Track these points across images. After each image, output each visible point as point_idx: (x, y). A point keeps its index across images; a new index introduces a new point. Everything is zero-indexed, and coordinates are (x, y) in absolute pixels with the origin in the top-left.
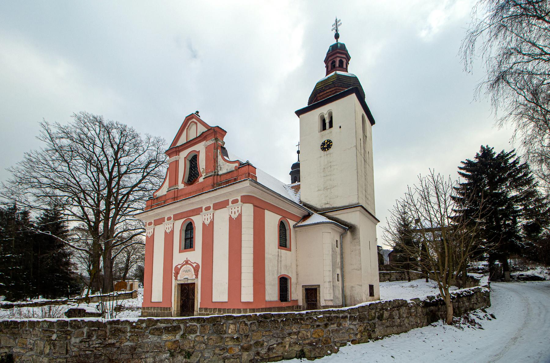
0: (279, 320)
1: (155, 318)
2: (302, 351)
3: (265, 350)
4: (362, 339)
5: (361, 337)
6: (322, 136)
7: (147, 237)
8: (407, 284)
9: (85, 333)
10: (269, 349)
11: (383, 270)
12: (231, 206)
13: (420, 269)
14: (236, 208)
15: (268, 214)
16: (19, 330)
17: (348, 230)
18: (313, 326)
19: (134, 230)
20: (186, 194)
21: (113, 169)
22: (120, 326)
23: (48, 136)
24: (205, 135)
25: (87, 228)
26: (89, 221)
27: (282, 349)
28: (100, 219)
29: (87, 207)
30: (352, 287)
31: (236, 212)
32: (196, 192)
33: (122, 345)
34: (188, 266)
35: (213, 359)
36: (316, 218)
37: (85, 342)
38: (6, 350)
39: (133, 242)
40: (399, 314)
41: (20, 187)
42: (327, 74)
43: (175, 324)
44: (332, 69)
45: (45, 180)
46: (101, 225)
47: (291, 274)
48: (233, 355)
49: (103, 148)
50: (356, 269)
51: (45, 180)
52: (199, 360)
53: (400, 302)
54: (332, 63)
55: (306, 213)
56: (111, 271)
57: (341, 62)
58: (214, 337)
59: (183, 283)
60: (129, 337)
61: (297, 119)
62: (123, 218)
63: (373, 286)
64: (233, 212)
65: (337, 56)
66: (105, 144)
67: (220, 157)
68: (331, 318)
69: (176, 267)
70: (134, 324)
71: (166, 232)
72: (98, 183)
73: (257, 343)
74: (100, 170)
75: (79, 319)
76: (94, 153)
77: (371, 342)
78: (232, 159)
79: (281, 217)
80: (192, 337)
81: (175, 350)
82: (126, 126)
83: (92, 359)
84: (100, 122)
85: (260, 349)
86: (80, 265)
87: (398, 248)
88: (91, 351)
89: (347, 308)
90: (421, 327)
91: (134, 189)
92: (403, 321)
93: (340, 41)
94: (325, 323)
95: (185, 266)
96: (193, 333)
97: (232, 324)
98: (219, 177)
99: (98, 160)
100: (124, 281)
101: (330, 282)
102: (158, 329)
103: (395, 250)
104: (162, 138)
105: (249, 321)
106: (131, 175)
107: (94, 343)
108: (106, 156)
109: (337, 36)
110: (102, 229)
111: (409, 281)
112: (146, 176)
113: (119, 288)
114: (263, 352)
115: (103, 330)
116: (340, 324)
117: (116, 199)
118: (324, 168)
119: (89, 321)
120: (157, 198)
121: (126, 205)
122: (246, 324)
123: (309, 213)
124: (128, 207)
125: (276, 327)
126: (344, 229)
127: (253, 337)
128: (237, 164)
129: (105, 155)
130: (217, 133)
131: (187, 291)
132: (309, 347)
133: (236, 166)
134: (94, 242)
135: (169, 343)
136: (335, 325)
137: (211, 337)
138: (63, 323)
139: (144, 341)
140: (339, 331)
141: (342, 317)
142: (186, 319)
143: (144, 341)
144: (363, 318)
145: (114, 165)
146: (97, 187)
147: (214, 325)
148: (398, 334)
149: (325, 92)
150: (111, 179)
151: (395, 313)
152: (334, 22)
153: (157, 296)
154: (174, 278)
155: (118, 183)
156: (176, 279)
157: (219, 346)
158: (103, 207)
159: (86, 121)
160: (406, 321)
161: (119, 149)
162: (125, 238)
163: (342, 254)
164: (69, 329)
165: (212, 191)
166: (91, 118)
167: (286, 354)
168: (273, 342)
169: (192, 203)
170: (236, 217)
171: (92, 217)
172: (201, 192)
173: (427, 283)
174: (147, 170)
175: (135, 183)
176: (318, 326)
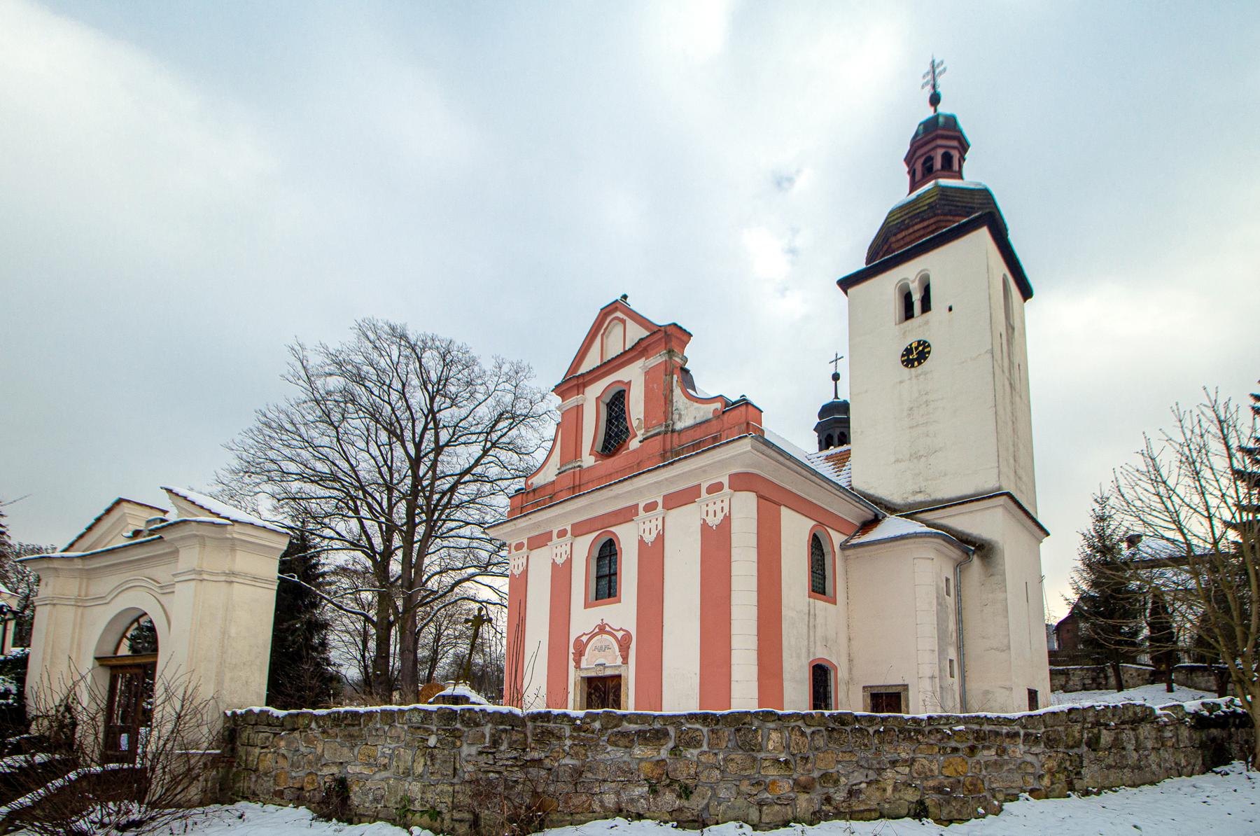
0: (871, 731)
2: (921, 803)
4: (1054, 790)
5: (1053, 783)
13: (1146, 658)
16: (361, 730)
17: (974, 552)
18: (944, 748)
20: (600, 479)
21: (422, 436)
22: (551, 725)
23: (302, 373)
24: (644, 344)
27: (878, 794)
30: (986, 693)
31: (719, 511)
32: (623, 471)
34: (605, 636)
36: (893, 526)
37: (488, 753)
38: (335, 770)
40: (1137, 739)
41: (247, 479)
43: (657, 726)
44: (924, 176)
45: (293, 467)
47: (837, 659)
50: (997, 649)
51: (293, 467)
52: (708, 805)
53: (1138, 710)
55: (870, 516)
57: (947, 159)
58: (738, 756)
59: (593, 674)
60: (570, 747)
63: (1036, 692)
67: (677, 392)
69: (578, 639)
70: (578, 722)
71: (554, 564)
72: (390, 469)
73: (825, 776)
77: (1074, 797)
80: (692, 753)
84: (403, 337)
85: (832, 790)
92: (1146, 756)
93: (943, 108)
94: (970, 744)
96: (695, 747)
98: (676, 435)
102: (625, 734)
108: (409, 407)
109: (935, 100)
112: (489, 450)
114: (839, 797)
116: (1004, 751)
117: (428, 499)
118: (911, 409)
119: (495, 712)
120: (534, 490)
122: (803, 734)
123: (876, 516)
124: (448, 519)
125: (866, 745)
126: (966, 552)
128: (718, 405)
130: (671, 338)
132: (936, 797)
136: (993, 752)
139: (598, 758)
140: (1001, 766)
141: (1008, 735)
143: (598, 758)
144: (1055, 740)
145: (425, 429)
147: (738, 730)
148: (1134, 785)
152: (928, 68)
154: (572, 664)
155: (433, 466)
156: (578, 666)
157: (748, 777)
160: (1153, 757)
163: (959, 612)
164: (458, 726)
167: (887, 806)
168: (858, 777)
169: (616, 497)
170: (717, 522)
172: (636, 471)
175: (467, 466)
176: (955, 750)
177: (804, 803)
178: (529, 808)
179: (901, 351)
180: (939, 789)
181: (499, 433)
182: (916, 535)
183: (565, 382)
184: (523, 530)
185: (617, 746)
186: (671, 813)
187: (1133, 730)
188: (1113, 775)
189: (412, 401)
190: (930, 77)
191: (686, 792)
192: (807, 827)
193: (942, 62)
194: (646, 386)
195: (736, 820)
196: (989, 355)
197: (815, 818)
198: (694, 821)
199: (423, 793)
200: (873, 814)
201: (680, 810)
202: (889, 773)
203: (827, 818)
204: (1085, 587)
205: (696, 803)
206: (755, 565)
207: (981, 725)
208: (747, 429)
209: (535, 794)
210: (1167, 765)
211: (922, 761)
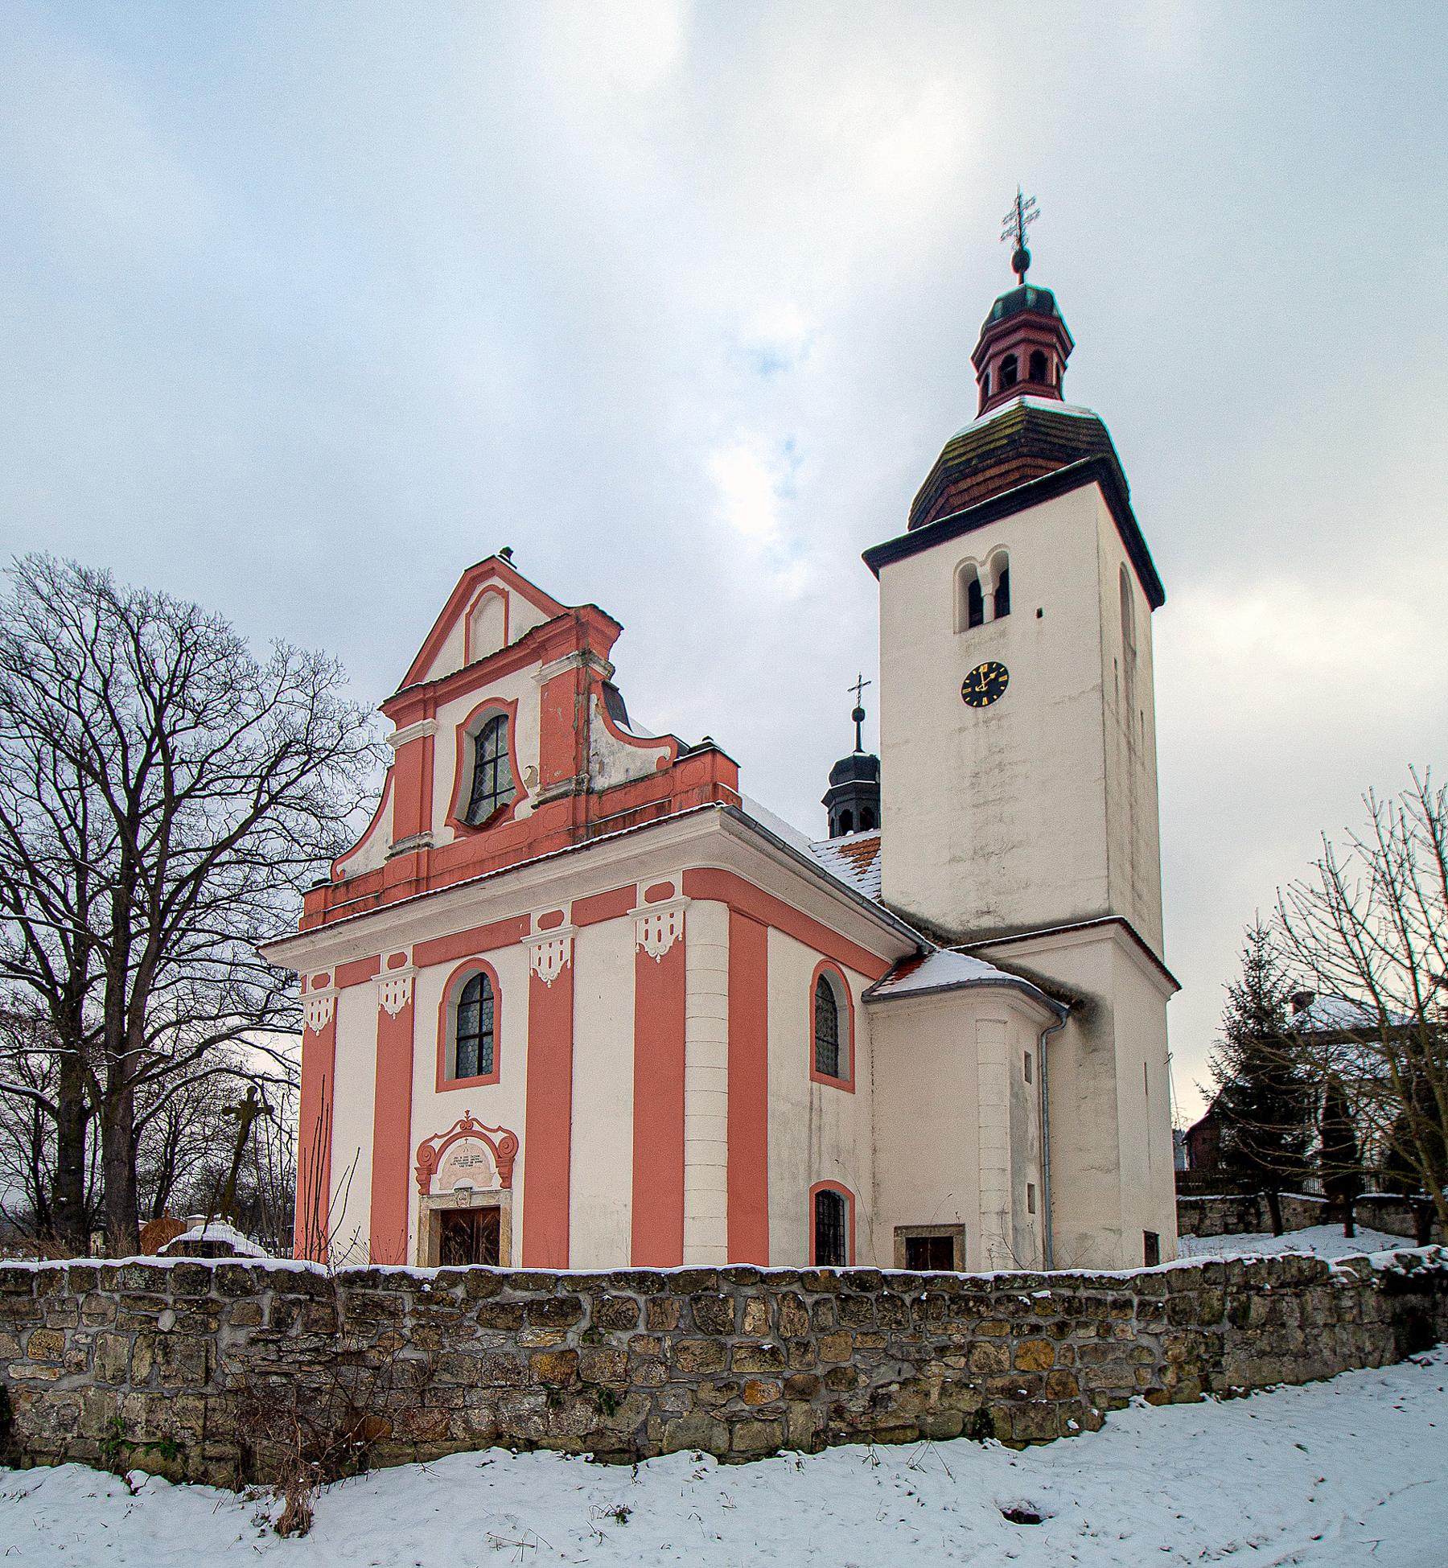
0: (908, 1300)
2: (982, 1413)
3: (862, 1402)
5: (1179, 1380)
6: (968, 650)
9: (267, 1312)
13: (1316, 1185)
14: (666, 918)
15: (776, 941)
16: (34, 1301)
18: (1019, 1326)
20: (464, 868)
22: (380, 1292)
24: (540, 637)
27: (917, 1401)
30: (1084, 1237)
31: (666, 932)
32: (504, 856)
36: (946, 967)
40: (1303, 1311)
43: (562, 1293)
52: (645, 1424)
53: (1305, 1265)
54: (1002, 368)
55: (910, 950)
57: (1039, 365)
58: (696, 1342)
59: (452, 1205)
64: (653, 935)
65: (1024, 338)
67: (598, 724)
69: (425, 1145)
71: (382, 1011)
72: (82, 833)
80: (619, 1339)
81: (564, 1385)
85: (846, 1396)
88: (286, 1375)
92: (1316, 1337)
95: (461, 1141)
96: (625, 1329)
98: (594, 798)
102: (505, 1308)
109: (1021, 262)
114: (856, 1406)
116: (1109, 1329)
117: (154, 891)
118: (976, 775)
120: (347, 884)
122: (800, 1305)
123: (919, 948)
125: (899, 1323)
126: (1057, 1013)
127: (824, 1350)
128: (666, 751)
130: (585, 631)
132: (1006, 1404)
135: (545, 1359)
137: (686, 1343)
138: (196, 1273)
139: (461, 1347)
140: (1104, 1353)
143: (461, 1347)
144: (1183, 1311)
145: (147, 763)
148: (1298, 1382)
152: (1011, 207)
154: (415, 1187)
155: (163, 832)
156: (425, 1191)
157: (711, 1377)
160: (1325, 1338)
163: (1044, 1108)
164: (214, 1294)
167: (930, 1420)
168: (885, 1373)
169: (492, 901)
170: (664, 951)
171: (59, 964)
173: (1350, 1241)
176: (1035, 1329)
180: (1010, 1392)
181: (284, 779)
183: (402, 693)
184: (328, 952)
185: (493, 1327)
187: (1297, 1295)
188: (1268, 1367)
190: (1013, 223)
191: (609, 1403)
194: (544, 711)
196: (1098, 694)
197: (818, 1442)
198: (622, 1451)
199: (150, 1411)
201: (600, 1432)
202: (934, 1368)
203: (837, 1441)
204: (1230, 1073)
205: (626, 1421)
206: (724, 1026)
207: (1075, 1289)
209: (352, 1411)
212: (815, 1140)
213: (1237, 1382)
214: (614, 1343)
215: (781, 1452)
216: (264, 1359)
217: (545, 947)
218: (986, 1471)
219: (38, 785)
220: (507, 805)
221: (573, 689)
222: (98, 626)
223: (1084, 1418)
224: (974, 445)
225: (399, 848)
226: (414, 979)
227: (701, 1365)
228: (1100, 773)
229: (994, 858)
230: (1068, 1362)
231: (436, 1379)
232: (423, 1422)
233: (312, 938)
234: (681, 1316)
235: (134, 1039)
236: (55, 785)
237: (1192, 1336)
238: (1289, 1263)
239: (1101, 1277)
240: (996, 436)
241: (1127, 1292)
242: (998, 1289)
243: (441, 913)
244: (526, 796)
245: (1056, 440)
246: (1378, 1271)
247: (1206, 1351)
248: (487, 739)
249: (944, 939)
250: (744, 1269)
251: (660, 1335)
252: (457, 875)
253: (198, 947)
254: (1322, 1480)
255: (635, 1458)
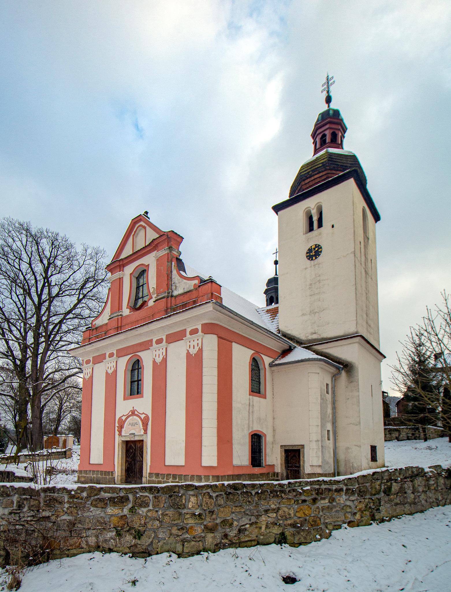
0: (253, 492)
1: (98, 486)
2: (283, 534)
5: (362, 517)
6: (308, 240)
7: (84, 379)
8: (422, 444)
10: (240, 531)
11: (389, 425)
12: (189, 338)
13: (440, 424)
15: (236, 348)
17: (342, 369)
18: (298, 501)
19: (68, 369)
20: (132, 323)
22: (56, 495)
25: (12, 367)
26: (14, 359)
27: (256, 530)
28: (28, 356)
29: (13, 340)
30: (347, 448)
32: (145, 319)
33: (59, 519)
34: (135, 417)
35: (170, 541)
36: (300, 353)
37: (15, 513)
39: (66, 385)
40: (413, 486)
42: (316, 151)
43: (122, 494)
46: (29, 363)
48: (194, 537)
49: (30, 264)
50: (353, 424)
52: (152, 542)
53: (414, 470)
54: (321, 138)
55: (286, 347)
56: (41, 424)
57: (334, 136)
58: (170, 512)
59: (128, 439)
61: (274, 217)
62: (54, 355)
64: (192, 347)
65: (330, 128)
66: (32, 259)
67: (174, 272)
68: (321, 491)
69: (120, 419)
70: (73, 493)
71: (107, 373)
72: (25, 309)
74: (27, 293)
75: (8, 484)
76: (20, 270)
77: (374, 524)
78: (190, 274)
79: (253, 352)
80: (143, 511)
82: (57, 234)
83: (23, 535)
84: (27, 230)
85: (228, 530)
86: (4, 415)
87: (410, 394)
88: (23, 525)
89: (341, 478)
90: (443, 506)
91: (68, 317)
92: (419, 496)
94: (313, 497)
95: (131, 417)
96: (145, 507)
97: (193, 495)
98: (173, 299)
99: (25, 279)
100: (56, 435)
101: (318, 441)
102: (102, 500)
103: (407, 397)
104: (101, 248)
105: (214, 492)
106: (64, 299)
107: (26, 515)
108: (34, 274)
109: (328, 100)
110: (30, 367)
111: (426, 440)
112: (81, 300)
113: (51, 444)
114: (232, 533)
115: (37, 500)
118: (311, 285)
119: (19, 488)
120: (96, 328)
121: (58, 338)
122: (211, 497)
123: (290, 347)
125: (249, 502)
126: (338, 368)
128: (196, 282)
129: (33, 272)
130: (171, 240)
131: (133, 451)
132: (292, 530)
133: (195, 284)
134: (20, 385)
136: (327, 501)
137: (167, 512)
139: (85, 515)
140: (332, 509)
142: (135, 488)
143: (85, 515)
144: (364, 491)
146: (23, 314)
147: (171, 496)
148: (411, 514)
149: (313, 178)
150: (40, 304)
151: (408, 485)
152: (325, 80)
153: (97, 456)
154: (117, 433)
155: (48, 309)
156: (120, 434)
157: (176, 525)
158: (30, 340)
159: (11, 229)
160: (423, 496)
161: (49, 264)
162: (56, 381)
163: (334, 402)
165: (165, 317)
166: (17, 225)
167: (262, 537)
168: (245, 520)
169: (140, 335)
170: (195, 352)
171: (18, 353)
174: (83, 292)
175: (69, 309)
176: (304, 501)
177: (210, 539)
178: (41, 547)
179: (306, 250)
180: (294, 525)
181: (88, 290)
182: (309, 360)
183: (112, 263)
184: (90, 352)
185: (96, 507)
186: (129, 548)
187: (411, 481)
188: (399, 509)
189: (36, 269)
190: (325, 86)
191: (139, 535)
192: (211, 554)
193: (333, 77)
194: (157, 268)
195: (168, 551)
196: (353, 255)
197: (216, 548)
198: (143, 552)
200: (253, 543)
201: (135, 545)
202: (263, 518)
203: (224, 547)
204: (409, 384)
205: (145, 541)
206: (216, 378)
207: (320, 485)
208: (212, 297)
209: (44, 538)
210: (431, 500)
211: (284, 508)
212: (251, 416)
213: (386, 516)
214: (141, 513)
215: (202, 553)
216: (14, 520)
217: (157, 351)
218: (278, 559)
219: (11, 293)
220: (146, 301)
221: (166, 260)
222: (27, 240)
223: (323, 534)
224: (310, 167)
225: (112, 316)
226: (117, 362)
227: (172, 520)
228: (354, 283)
229: (317, 314)
230: (317, 513)
231: (76, 526)
232: (72, 541)
233: (84, 347)
234: (165, 502)
235: (41, 378)
236: (16, 293)
237: (367, 500)
238: (408, 470)
239: (331, 480)
240: (318, 163)
241: (341, 485)
242: (289, 487)
243: (124, 339)
244: (152, 298)
245: (339, 164)
246: (445, 470)
247: (373, 505)
248: (140, 278)
249: (300, 343)
250: (189, 485)
251: (157, 509)
252: (130, 325)
253: (63, 346)
254: (410, 561)
255: (148, 555)
